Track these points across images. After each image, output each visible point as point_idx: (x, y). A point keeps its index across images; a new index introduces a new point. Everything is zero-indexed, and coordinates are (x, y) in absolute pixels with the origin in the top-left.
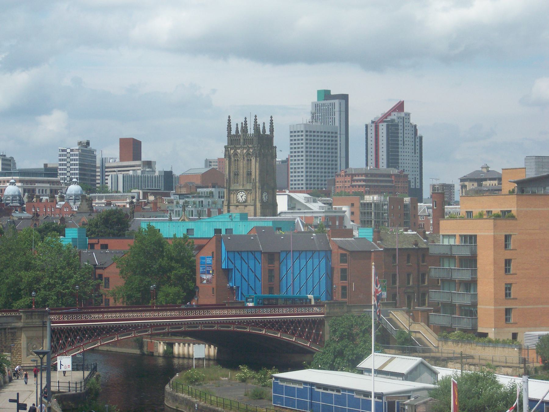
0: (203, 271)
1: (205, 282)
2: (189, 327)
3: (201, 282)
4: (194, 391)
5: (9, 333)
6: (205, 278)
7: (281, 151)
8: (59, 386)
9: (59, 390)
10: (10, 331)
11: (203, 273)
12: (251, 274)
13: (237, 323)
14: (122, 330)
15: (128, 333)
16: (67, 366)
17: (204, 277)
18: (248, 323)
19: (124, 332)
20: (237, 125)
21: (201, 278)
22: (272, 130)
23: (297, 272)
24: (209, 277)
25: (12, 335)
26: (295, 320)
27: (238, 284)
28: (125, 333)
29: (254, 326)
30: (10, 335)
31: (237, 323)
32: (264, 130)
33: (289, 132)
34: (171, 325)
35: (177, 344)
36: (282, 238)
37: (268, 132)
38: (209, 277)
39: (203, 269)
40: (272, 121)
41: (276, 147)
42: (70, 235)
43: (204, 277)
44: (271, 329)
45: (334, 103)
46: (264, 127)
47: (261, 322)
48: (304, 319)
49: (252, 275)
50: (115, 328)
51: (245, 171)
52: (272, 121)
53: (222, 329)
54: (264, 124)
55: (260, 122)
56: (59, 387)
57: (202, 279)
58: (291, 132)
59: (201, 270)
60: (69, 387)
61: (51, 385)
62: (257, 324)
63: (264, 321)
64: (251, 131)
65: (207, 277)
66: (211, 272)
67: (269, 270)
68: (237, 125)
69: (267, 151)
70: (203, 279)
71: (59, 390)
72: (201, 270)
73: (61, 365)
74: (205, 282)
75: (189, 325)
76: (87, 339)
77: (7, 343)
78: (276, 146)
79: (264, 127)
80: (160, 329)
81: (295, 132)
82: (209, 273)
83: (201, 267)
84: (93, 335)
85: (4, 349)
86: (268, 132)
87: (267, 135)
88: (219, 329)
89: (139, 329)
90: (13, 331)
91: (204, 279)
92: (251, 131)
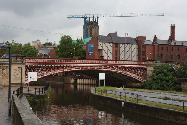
1: (90, 54)
3: (89, 55)
6: (90, 53)
9: (29, 93)
11: (90, 51)
12: (106, 52)
17: (90, 52)
18: (116, 68)
21: (88, 53)
29: (118, 69)
30: (5, 67)
32: (96, 20)
37: (97, 21)
38: (92, 52)
43: (90, 52)
46: (96, 19)
50: (53, 67)
51: (90, 32)
53: (76, 69)
57: (89, 54)
61: (125, 37)
62: (123, 69)
67: (116, 50)
71: (29, 93)
73: (30, 77)
74: (90, 54)
76: (44, 72)
79: (96, 19)
82: (92, 51)
84: (51, 69)
86: (97, 21)
91: (90, 54)
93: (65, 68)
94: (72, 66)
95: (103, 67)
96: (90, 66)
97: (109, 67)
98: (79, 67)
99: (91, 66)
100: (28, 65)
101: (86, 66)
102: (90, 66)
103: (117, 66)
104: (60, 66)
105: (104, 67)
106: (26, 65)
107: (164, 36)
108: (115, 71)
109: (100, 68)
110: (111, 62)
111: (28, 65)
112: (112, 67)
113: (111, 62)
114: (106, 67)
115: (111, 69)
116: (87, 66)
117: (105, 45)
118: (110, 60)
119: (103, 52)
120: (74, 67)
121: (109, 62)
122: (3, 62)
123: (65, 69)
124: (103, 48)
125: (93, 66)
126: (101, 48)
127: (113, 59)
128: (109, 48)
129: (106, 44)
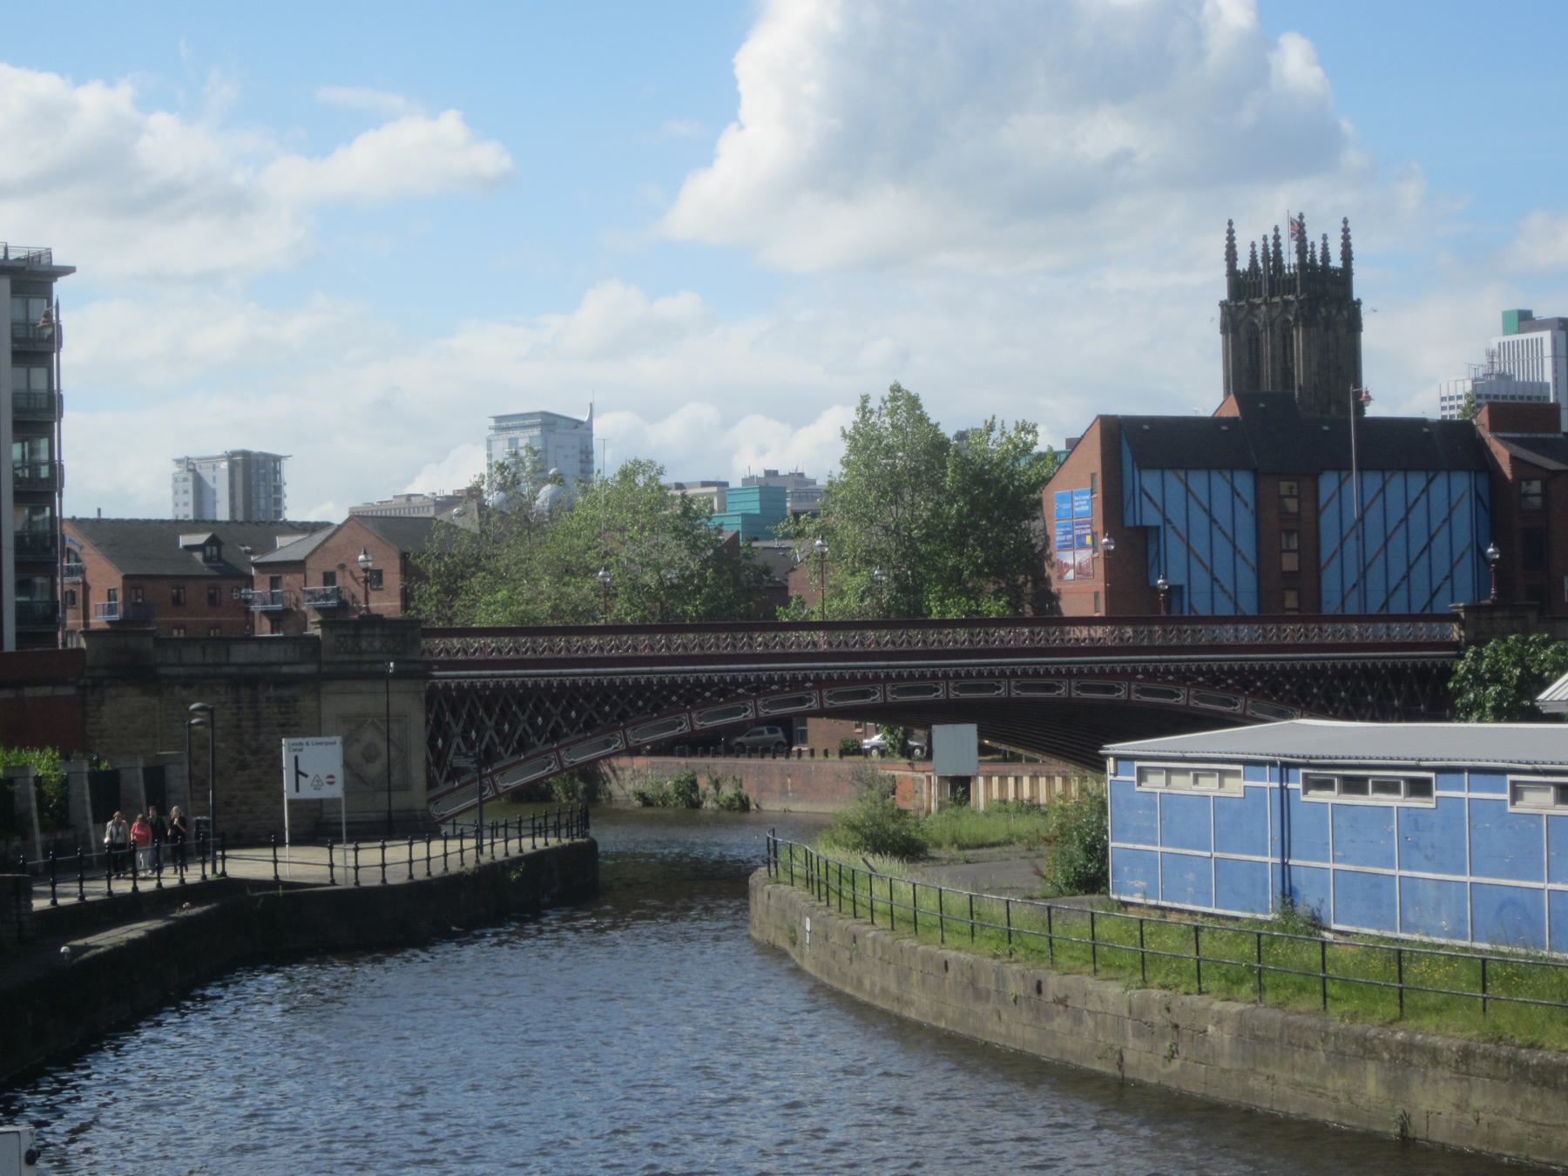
0: (1066, 541)
1: (1070, 574)
2: (963, 689)
4: (929, 903)
5: (268, 699)
6: (1070, 561)
7: (1375, 311)
8: (272, 865)
10: (272, 692)
13: (1140, 676)
14: (708, 694)
15: (730, 706)
16: (324, 780)
17: (1068, 558)
18: (1183, 677)
19: (718, 703)
20: (1253, 245)
22: (1347, 256)
23: (1374, 544)
24: (1084, 556)
25: (283, 710)
26: (1354, 666)
27: (1178, 578)
28: (718, 709)
31: (1140, 676)
32: (1326, 256)
33: (1438, 399)
34: (894, 680)
35: (981, 780)
36: (1326, 428)
38: (1084, 556)
39: (1066, 533)
40: (1346, 230)
41: (1359, 302)
42: (737, 507)
43: (1068, 558)
44: (1268, 697)
45: (1542, 339)
47: (1231, 672)
48: (1384, 665)
49: (1199, 519)
50: (681, 686)
52: (1346, 230)
53: (963, 695)
54: (1325, 237)
55: (1313, 236)
56: (276, 862)
58: (1443, 399)
59: (1058, 538)
60: (276, 862)
63: (1242, 669)
64: (1290, 259)
65: (1078, 559)
66: (1088, 540)
68: (1253, 245)
69: (1334, 312)
70: (1066, 565)
72: (1058, 538)
73: (298, 773)
75: (962, 682)
77: (262, 738)
78: (1359, 300)
80: (855, 695)
81: (1451, 398)
82: (1083, 546)
83: (1059, 526)
85: (249, 758)
87: (1336, 270)
88: (1073, 695)
89: (773, 693)
90: (285, 693)
92: (1290, 259)
93: (739, 696)
94: (806, 679)
95: (1069, 674)
96: (900, 676)
97: (1129, 676)
98: (865, 679)
99: (969, 675)
100: (1324, 666)
101: (1047, 673)
102: (900, 676)
103: (1246, 666)
104: (710, 684)
105: (1080, 674)
106: (434, 686)
107: (93, 515)
108: (1181, 700)
109: (1049, 681)
110: (1246, 633)
111: (1324, 666)
112: (1151, 676)
113: (1246, 633)
114: (1091, 674)
115: (1144, 692)
116: (1058, 672)
117: (1228, 490)
118: (1238, 619)
119: (1174, 548)
120: (819, 683)
121: (1226, 634)
122: (257, 670)
123: (751, 703)
124: (1166, 521)
125: (980, 675)
126: (1151, 518)
127: (1260, 609)
128: (1222, 512)
129: (1198, 480)
